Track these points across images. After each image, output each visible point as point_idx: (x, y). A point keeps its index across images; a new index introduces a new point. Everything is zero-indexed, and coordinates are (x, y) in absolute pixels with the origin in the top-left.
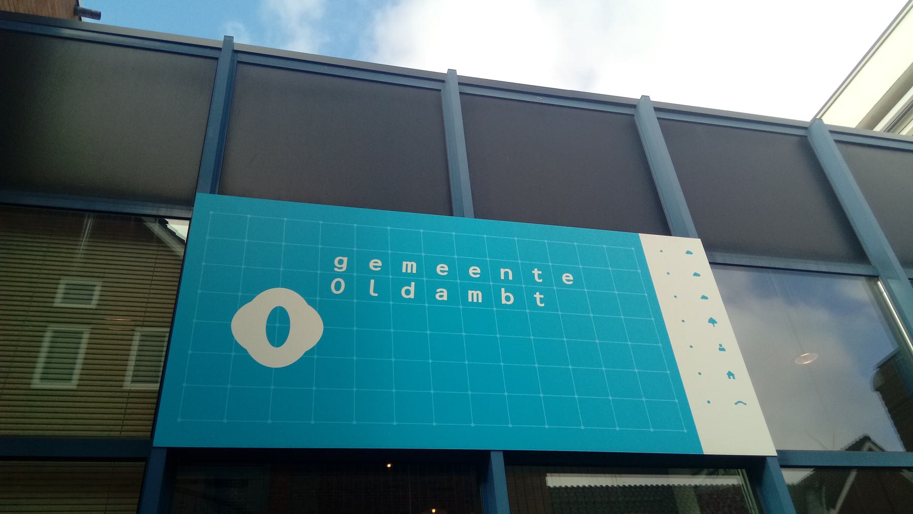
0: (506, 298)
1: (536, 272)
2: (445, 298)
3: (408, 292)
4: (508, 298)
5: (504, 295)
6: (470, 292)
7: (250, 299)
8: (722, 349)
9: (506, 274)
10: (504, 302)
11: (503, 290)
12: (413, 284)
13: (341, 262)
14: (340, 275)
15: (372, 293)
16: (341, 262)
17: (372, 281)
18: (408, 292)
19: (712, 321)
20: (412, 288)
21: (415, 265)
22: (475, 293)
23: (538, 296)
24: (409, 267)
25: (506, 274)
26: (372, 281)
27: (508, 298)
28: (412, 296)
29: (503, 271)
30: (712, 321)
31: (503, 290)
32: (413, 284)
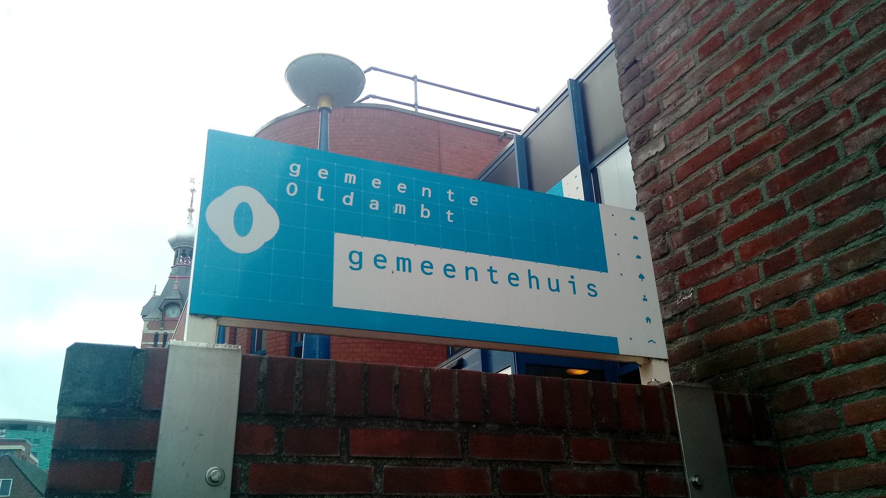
0: (425, 212)
1: (450, 193)
2: (377, 208)
3: (348, 200)
4: (425, 213)
5: (423, 210)
6: (347, 175)
7: (266, 244)
8: (645, 300)
9: (426, 192)
10: (422, 215)
11: (423, 206)
12: (352, 194)
13: (295, 168)
14: (292, 179)
15: (319, 198)
16: (295, 168)
17: (320, 188)
18: (348, 200)
19: (641, 277)
20: (351, 197)
21: (404, 207)
22: (351, 176)
23: (449, 213)
24: (350, 178)
25: (426, 192)
26: (320, 188)
27: (425, 213)
28: (351, 204)
29: (424, 189)
30: (641, 277)
31: (423, 206)
32: (352, 194)
